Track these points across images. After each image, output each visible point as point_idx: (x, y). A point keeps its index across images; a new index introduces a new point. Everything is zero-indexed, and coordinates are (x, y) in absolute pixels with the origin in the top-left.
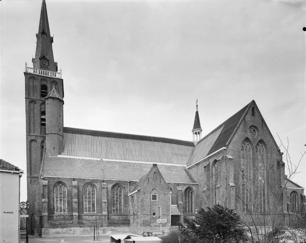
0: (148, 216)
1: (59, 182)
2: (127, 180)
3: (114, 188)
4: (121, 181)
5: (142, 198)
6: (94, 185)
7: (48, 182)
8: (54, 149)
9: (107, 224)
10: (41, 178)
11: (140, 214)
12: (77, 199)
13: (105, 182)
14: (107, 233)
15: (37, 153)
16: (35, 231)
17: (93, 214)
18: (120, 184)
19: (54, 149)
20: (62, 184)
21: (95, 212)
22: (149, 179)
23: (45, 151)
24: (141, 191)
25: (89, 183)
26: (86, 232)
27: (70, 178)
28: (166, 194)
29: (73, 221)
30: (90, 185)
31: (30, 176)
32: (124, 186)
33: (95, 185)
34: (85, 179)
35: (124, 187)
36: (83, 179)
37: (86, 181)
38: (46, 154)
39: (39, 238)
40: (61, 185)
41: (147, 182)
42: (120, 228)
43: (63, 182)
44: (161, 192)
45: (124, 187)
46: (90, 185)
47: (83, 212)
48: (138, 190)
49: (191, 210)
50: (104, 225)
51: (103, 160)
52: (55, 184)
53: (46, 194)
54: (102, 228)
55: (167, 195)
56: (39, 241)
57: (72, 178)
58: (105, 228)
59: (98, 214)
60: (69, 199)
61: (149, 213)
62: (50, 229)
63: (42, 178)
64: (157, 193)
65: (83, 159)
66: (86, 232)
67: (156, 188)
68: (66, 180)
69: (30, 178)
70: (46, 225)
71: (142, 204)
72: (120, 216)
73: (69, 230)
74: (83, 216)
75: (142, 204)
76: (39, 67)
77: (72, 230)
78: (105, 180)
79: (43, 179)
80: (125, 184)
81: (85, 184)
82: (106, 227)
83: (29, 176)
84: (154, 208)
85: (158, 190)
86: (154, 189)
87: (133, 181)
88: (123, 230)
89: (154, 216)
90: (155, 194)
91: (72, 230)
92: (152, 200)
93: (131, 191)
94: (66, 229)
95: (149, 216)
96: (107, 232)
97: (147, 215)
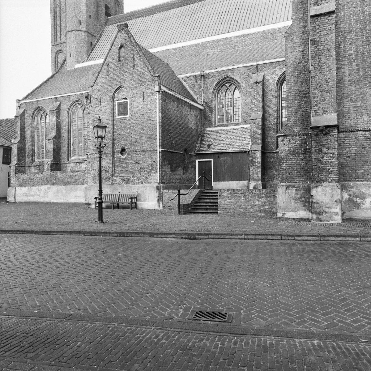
5: (94, 113)
24: (92, 99)
27: (52, 98)
34: (71, 95)
37: (72, 98)
84: (122, 135)
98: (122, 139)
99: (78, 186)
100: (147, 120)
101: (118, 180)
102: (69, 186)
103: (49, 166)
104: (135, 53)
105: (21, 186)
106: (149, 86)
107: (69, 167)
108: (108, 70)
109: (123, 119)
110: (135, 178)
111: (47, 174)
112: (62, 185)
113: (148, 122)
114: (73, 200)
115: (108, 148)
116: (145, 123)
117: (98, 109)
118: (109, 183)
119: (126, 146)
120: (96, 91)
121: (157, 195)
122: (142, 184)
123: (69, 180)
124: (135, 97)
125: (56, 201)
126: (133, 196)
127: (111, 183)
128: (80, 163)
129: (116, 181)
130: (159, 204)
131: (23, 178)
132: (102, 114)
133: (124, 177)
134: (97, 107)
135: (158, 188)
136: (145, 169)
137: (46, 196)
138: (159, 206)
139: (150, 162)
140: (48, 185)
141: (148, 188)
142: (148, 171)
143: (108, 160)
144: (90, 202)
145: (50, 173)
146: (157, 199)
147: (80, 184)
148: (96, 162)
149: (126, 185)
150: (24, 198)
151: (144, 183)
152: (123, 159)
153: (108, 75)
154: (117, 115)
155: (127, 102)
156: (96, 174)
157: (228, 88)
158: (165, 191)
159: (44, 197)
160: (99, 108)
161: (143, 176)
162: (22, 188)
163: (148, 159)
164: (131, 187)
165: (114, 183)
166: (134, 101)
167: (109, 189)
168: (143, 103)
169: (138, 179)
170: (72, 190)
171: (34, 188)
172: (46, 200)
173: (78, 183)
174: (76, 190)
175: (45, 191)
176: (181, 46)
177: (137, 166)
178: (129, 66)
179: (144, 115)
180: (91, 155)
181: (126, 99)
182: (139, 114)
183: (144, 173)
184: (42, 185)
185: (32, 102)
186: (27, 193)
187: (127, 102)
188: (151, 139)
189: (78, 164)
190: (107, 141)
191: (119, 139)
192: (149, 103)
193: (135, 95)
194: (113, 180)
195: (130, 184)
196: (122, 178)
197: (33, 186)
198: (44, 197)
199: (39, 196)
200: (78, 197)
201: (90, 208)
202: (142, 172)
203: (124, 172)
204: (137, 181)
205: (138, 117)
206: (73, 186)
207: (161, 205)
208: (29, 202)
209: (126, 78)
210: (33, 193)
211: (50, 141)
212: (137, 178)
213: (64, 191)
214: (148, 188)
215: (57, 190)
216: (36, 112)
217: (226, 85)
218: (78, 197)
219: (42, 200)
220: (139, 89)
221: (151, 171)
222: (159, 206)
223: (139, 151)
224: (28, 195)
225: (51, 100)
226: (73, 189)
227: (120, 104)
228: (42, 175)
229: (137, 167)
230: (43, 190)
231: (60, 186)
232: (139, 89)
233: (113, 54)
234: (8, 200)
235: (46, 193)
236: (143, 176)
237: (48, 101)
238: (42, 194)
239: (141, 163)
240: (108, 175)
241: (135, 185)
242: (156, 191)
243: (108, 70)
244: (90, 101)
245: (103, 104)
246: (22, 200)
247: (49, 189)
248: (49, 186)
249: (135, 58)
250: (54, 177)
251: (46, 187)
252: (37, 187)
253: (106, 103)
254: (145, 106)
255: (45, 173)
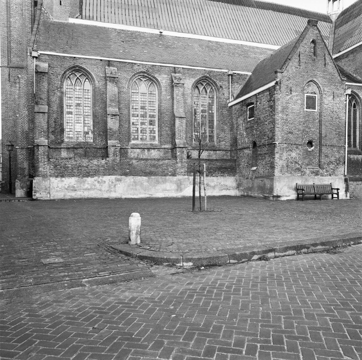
0: (297, 148)
1: (74, 67)
2: (226, 71)
3: (197, 87)
4: (214, 72)
5: (284, 101)
6: (154, 77)
7: (49, 66)
8: (61, 4)
9: (186, 169)
10: (31, 56)
11: (279, 141)
12: (117, 109)
13: (179, 72)
14: (187, 189)
15: (24, 17)
16: (17, 185)
17: (151, 145)
18: (211, 79)
19: (61, 4)
20: (81, 74)
21: (156, 142)
22: (299, 55)
23: (41, 9)
24: (282, 85)
25: (144, 72)
26: (138, 187)
27: (101, 60)
28: (338, 96)
29: (108, 159)
30: (145, 79)
31: (8, 65)
32: (219, 83)
33: (157, 80)
34: (135, 64)
35: (221, 87)
36: (129, 63)
37: (136, 67)
38: (42, 15)
39: (218, 257)
40: (78, 76)
41: (296, 64)
42: (215, 179)
43: (84, 69)
44: (326, 89)
45: (221, 87)
46: (145, 79)
47: (129, 140)
48: (277, 83)
49: (353, 142)
50: (178, 170)
51: (165, 33)
52: (64, 73)
53: (44, 88)
54: (175, 178)
55: (338, 99)
56: (211, 359)
57: (105, 60)
58: (180, 177)
59: (163, 147)
60: (97, 108)
61: (299, 141)
62: (53, 179)
63: (34, 57)
64: (318, 92)
65: (123, 30)
66: (138, 187)
67: (315, 80)
68: (91, 64)
69: (8, 69)
70: (44, 167)
71: (285, 117)
72: (212, 152)
73: (99, 182)
74: (129, 151)
75: (285, 117)
76: (9, 197)
77: (105, 182)
78: (178, 68)
79: (36, 58)
80: (221, 80)
81: (134, 75)
82: (185, 175)
83: (6, 65)
84: (310, 128)
85: (320, 85)
86: (311, 81)
87: (238, 74)
88: (222, 183)
89: (309, 150)
90: (312, 93)
91: (105, 182)
92: (305, 110)
93: (235, 95)
94: (93, 179)
95: (300, 147)
96: (185, 188)
97: (295, 144)
98: (310, 132)
99: (167, 177)
100: (336, 118)
101: (308, 172)
102: (153, 177)
103: (118, 150)
104: (326, 52)
105: (62, 176)
106: (338, 87)
107: (132, 154)
108: (300, 60)
109: (311, 112)
110: (324, 171)
111: (114, 160)
112: (141, 176)
113: (338, 120)
114: (160, 195)
115: (298, 139)
116: (334, 120)
117: (288, 97)
118: (298, 175)
119: (314, 139)
120: (286, 78)
121: (345, 186)
122: (331, 176)
123: (153, 169)
124: (325, 94)
125: (133, 197)
126: (300, 187)
127: (300, 174)
128: (149, 149)
129: (305, 173)
130: (346, 194)
131: (66, 164)
132: (292, 104)
133: (313, 169)
134: (287, 95)
135: (346, 180)
136: (334, 163)
137: (112, 190)
138: (346, 196)
139: (338, 157)
140: (116, 175)
141: (337, 180)
142: (336, 164)
143: (299, 152)
144: (279, 194)
145: (118, 159)
146: (344, 190)
147: (170, 175)
148: (285, 152)
149: (316, 177)
150: (69, 194)
151: (332, 175)
152: (310, 151)
153: (300, 66)
154: (305, 108)
155: (315, 97)
156: (284, 165)
157: (78, 78)
158: (351, 182)
159: (109, 191)
160: (289, 97)
161: (332, 169)
162: (63, 179)
163: (336, 153)
164: (322, 179)
165: (304, 175)
166: (325, 98)
167: (301, 181)
168: (333, 101)
169: (327, 171)
170: (158, 182)
171: (89, 180)
172: (113, 195)
173: (168, 174)
174: (165, 182)
175: (110, 183)
176: (175, 35)
177: (326, 159)
178: (320, 63)
179: (334, 113)
180: (280, 145)
181: (315, 94)
182: (329, 111)
183: (332, 166)
184: (105, 175)
185: (64, 57)
186: (75, 186)
187: (315, 97)
188: (339, 135)
189: (146, 151)
190: (297, 131)
191: (307, 131)
192: (338, 102)
193: (326, 93)
194: (302, 172)
195: (319, 176)
196: (311, 170)
197: (87, 176)
198: (109, 191)
199: (100, 190)
200: (168, 190)
201: (279, 200)
202: (330, 165)
203: (311, 164)
204: (326, 174)
205: (328, 114)
206: (160, 177)
207: (348, 195)
208: (80, 199)
209: (317, 73)
210: (86, 186)
211: (113, 117)
212: (326, 170)
213: (146, 184)
214: (337, 180)
215: (134, 182)
216: (68, 72)
217: (76, 74)
218: (168, 190)
219: (106, 195)
220: (329, 88)
221: (338, 164)
222: (346, 196)
223: (329, 146)
224: (77, 189)
225: (99, 61)
226: (160, 180)
227: (308, 98)
228: (103, 162)
229: (328, 160)
230: (107, 183)
231: (139, 177)
232: (329, 88)
233: (305, 46)
234: (34, 197)
235: (113, 187)
236: (332, 169)
237: (93, 62)
238: (105, 187)
239: (330, 156)
240: (297, 167)
241: (324, 177)
242: (343, 183)
243: (300, 60)
244: (279, 87)
245: (294, 94)
246: (64, 196)
247: (119, 180)
248: (119, 177)
249: (326, 58)
250: (126, 165)
251: (113, 177)
252: (96, 178)
253: (297, 93)
254: (335, 105)
255: (111, 158)
